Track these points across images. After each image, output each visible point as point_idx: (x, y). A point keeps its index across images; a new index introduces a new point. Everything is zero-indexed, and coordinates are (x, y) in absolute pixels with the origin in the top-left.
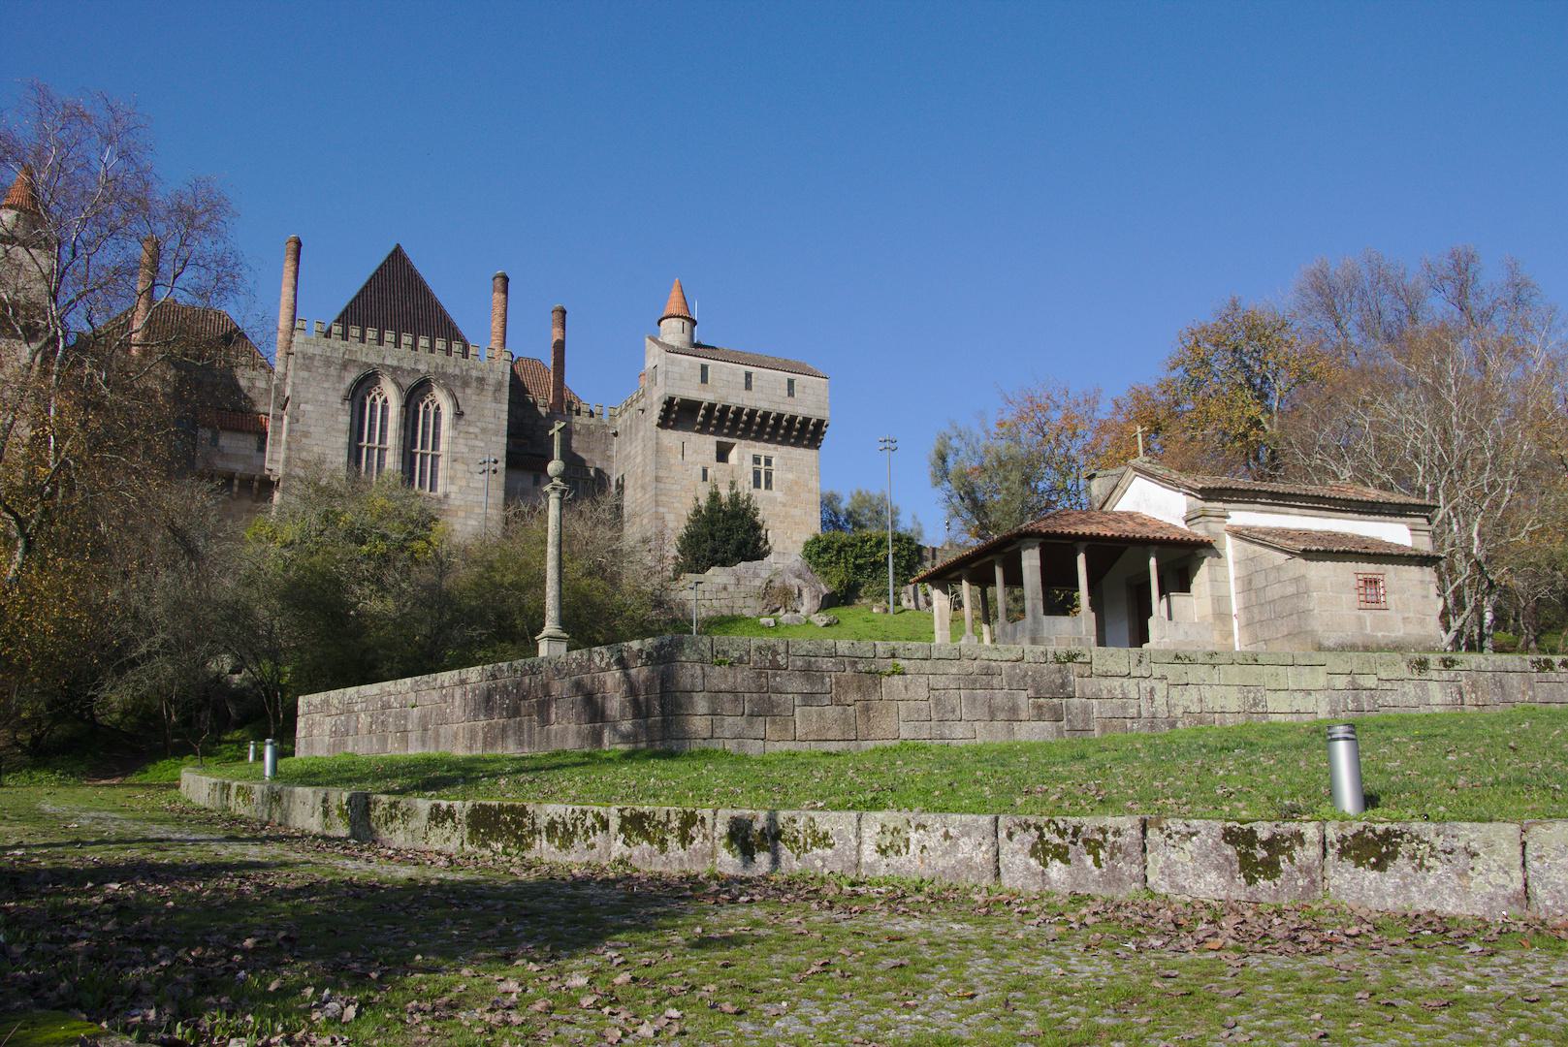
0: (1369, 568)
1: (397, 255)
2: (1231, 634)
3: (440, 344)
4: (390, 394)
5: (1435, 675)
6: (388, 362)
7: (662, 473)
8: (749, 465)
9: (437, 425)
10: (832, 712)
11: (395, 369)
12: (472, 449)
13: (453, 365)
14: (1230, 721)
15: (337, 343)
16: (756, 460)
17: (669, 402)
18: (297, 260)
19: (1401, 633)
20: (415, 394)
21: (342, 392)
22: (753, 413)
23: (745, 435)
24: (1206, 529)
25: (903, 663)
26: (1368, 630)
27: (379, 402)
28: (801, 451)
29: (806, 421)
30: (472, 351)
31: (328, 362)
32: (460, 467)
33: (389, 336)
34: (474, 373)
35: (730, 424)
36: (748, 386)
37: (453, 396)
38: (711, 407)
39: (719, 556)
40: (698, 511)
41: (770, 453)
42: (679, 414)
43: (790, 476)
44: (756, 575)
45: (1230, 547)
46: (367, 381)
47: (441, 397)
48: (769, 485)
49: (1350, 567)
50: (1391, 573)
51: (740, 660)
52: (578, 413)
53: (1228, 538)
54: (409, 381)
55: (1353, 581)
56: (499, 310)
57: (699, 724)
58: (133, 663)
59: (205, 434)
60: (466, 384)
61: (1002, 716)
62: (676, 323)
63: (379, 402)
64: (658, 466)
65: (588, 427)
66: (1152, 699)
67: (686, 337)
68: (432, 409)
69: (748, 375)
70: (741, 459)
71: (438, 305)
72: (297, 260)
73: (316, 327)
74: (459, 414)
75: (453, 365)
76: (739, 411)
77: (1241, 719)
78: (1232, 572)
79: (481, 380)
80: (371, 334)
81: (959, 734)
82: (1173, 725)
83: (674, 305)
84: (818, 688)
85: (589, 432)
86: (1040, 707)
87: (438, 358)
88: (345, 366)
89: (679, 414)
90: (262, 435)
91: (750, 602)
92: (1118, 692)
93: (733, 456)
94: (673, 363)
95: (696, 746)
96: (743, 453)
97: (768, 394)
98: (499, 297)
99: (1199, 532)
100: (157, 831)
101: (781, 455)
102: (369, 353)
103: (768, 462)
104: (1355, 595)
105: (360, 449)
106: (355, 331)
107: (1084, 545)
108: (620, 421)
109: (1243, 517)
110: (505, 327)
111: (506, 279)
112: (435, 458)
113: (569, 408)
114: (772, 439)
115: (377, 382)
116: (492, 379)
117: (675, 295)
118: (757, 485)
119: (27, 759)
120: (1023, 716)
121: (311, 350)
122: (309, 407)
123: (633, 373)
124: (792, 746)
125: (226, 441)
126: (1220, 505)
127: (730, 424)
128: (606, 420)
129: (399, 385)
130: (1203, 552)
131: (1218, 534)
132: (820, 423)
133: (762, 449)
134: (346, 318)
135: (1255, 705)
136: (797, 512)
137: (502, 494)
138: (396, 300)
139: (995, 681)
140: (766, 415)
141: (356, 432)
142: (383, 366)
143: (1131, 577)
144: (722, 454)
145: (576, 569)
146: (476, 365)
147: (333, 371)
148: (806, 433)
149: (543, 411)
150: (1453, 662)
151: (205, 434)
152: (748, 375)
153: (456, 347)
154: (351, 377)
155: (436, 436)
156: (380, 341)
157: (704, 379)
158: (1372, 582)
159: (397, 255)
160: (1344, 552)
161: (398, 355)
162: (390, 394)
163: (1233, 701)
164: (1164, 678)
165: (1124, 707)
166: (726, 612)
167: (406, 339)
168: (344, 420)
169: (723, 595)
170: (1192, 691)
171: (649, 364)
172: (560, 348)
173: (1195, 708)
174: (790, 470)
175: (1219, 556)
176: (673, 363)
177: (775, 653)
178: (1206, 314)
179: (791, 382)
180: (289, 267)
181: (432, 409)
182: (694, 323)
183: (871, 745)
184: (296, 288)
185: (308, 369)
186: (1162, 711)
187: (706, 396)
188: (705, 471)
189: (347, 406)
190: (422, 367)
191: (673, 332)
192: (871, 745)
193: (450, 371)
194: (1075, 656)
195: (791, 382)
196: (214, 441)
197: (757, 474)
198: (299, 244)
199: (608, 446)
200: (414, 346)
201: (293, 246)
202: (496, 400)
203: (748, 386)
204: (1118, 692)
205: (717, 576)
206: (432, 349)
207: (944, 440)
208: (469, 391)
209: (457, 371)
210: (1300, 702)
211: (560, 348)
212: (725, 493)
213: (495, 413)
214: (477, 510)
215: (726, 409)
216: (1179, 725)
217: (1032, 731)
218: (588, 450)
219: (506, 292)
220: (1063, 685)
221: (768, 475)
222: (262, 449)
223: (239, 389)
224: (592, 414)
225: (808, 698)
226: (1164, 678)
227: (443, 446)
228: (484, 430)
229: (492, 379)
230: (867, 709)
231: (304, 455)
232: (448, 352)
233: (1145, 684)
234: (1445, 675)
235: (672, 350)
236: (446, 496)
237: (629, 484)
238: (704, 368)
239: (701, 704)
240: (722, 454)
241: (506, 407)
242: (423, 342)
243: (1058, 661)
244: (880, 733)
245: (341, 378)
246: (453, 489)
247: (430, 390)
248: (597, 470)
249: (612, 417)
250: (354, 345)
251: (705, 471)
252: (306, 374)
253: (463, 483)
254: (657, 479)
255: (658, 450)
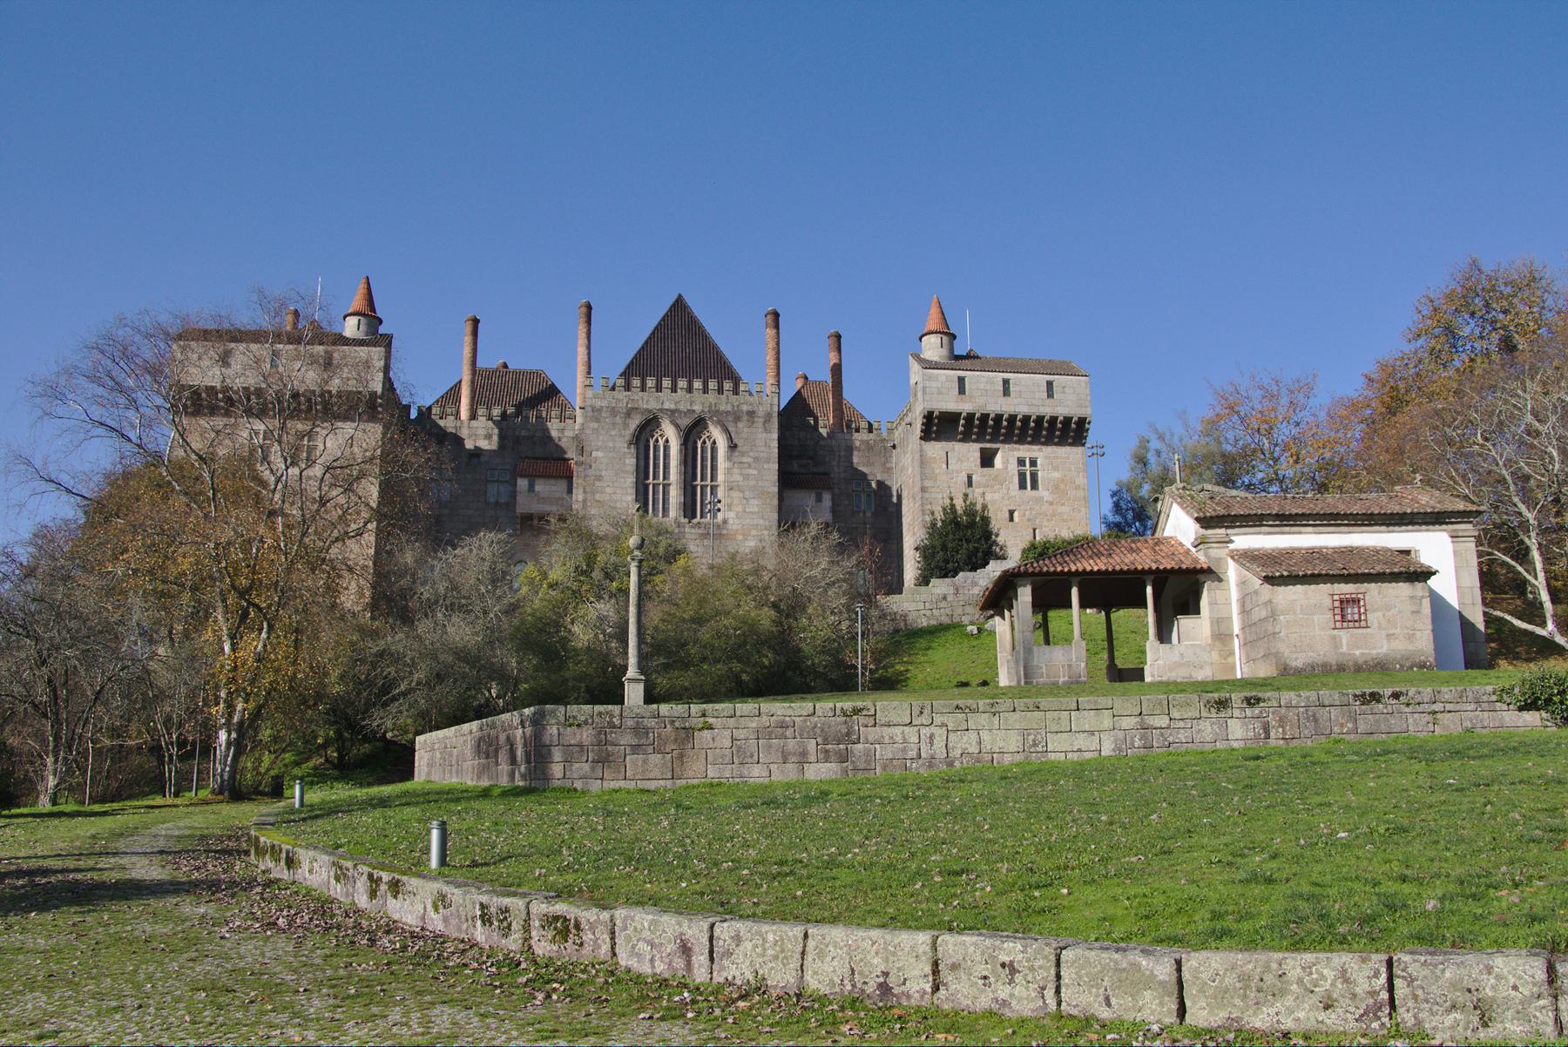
0: (1347, 589)
1: (679, 307)
2: (1232, 653)
3: (712, 384)
4: (670, 434)
5: (1237, 713)
6: (666, 406)
7: (927, 483)
8: (1013, 468)
9: (714, 458)
10: (655, 758)
11: (673, 412)
12: (746, 477)
13: (725, 403)
14: (1007, 759)
15: (621, 395)
16: (1021, 462)
17: (929, 417)
18: (589, 322)
19: (1384, 650)
20: (692, 432)
21: (628, 438)
22: (1012, 418)
23: (1008, 439)
24: (1206, 555)
25: (711, 720)
26: (1344, 649)
27: (661, 443)
28: (1067, 449)
29: (1067, 420)
30: (742, 388)
31: (613, 412)
32: (735, 494)
33: (666, 383)
34: (745, 408)
35: (990, 431)
36: (1006, 392)
37: (726, 430)
38: (970, 417)
39: (950, 566)
40: (933, 525)
41: (1034, 455)
42: (939, 426)
43: (1056, 475)
44: (975, 584)
45: (1232, 571)
46: (649, 425)
47: (716, 433)
48: (1035, 486)
49: (1325, 588)
50: (1373, 593)
51: (586, 722)
52: (857, 430)
53: (1231, 565)
54: (685, 422)
55: (1328, 602)
56: (771, 344)
57: (557, 770)
58: (394, 699)
59: (522, 483)
60: (737, 419)
61: (794, 759)
62: (933, 340)
63: (661, 443)
64: (923, 477)
65: (867, 442)
66: (932, 744)
67: (945, 352)
68: (709, 444)
69: (1006, 382)
70: (1006, 463)
71: (715, 347)
72: (589, 322)
73: (603, 382)
74: (733, 447)
75: (725, 403)
76: (999, 418)
77: (1019, 758)
78: (1234, 595)
79: (751, 414)
80: (651, 382)
81: (756, 774)
82: (951, 764)
83: (933, 322)
84: (643, 741)
85: (869, 447)
86: (827, 751)
87: (712, 397)
88: (629, 414)
89: (939, 426)
90: (568, 477)
91: (969, 609)
92: (899, 739)
93: (998, 460)
94: (930, 378)
95: (556, 783)
96: (1007, 457)
97: (1028, 397)
98: (771, 332)
99: (1202, 559)
100: (71, 864)
101: (1051, 459)
102: (649, 401)
103: (1033, 463)
104: (1329, 615)
105: (646, 487)
106: (636, 382)
107: (1075, 580)
108: (896, 434)
109: (1246, 540)
110: (778, 359)
111: (776, 315)
112: (714, 489)
113: (849, 427)
114: (1035, 441)
115: (659, 425)
116: (761, 411)
117: (934, 311)
118: (1022, 486)
119: (336, 772)
120: (812, 758)
121: (598, 403)
122: (600, 454)
123: (900, 388)
124: (622, 784)
125: (541, 486)
126: (1223, 531)
127: (990, 431)
128: (885, 435)
129: (677, 426)
130: (1201, 577)
131: (1219, 560)
132: (1082, 422)
133: (1026, 451)
134: (627, 374)
135: (1035, 745)
136: (1065, 509)
137: (776, 516)
138: (679, 347)
139: (789, 733)
140: (1026, 419)
141: (642, 472)
142: (661, 410)
143: (1180, 591)
144: (987, 460)
145: (655, 614)
146: (744, 403)
147: (618, 419)
148: (1070, 431)
149: (824, 432)
150: (1258, 700)
151: (522, 483)
152: (1006, 382)
153: (727, 385)
154: (635, 422)
155: (714, 468)
156: (659, 388)
157: (962, 390)
158: (1344, 602)
159: (679, 307)
160: (1313, 575)
161: (676, 399)
162: (670, 434)
163: (1012, 742)
164: (944, 725)
165: (904, 750)
166: (945, 620)
167: (682, 383)
168: (631, 462)
169: (943, 604)
170: (973, 736)
171: (912, 382)
172: (837, 370)
173: (974, 749)
174: (1056, 469)
175: (1220, 580)
176: (930, 378)
177: (612, 716)
178: (1440, 280)
179: (1050, 384)
180: (582, 328)
181: (709, 444)
182: (953, 337)
183: (684, 782)
184: (589, 347)
185: (598, 421)
186: (941, 753)
187: (965, 407)
188: (970, 478)
189: (633, 450)
190: (697, 408)
191: (932, 348)
192: (684, 782)
193: (722, 408)
194: (860, 710)
195: (1050, 384)
196: (531, 488)
197: (1022, 476)
198: (589, 307)
199: (887, 459)
200: (690, 390)
201: (584, 310)
202: (766, 430)
203: (1006, 392)
204: (899, 739)
205: (939, 586)
206: (705, 390)
207: (1144, 442)
208: (740, 425)
209: (729, 408)
210: (1081, 742)
211: (837, 370)
212: (959, 504)
213: (766, 442)
214: (754, 532)
215: (985, 417)
216: (957, 764)
217: (820, 772)
218: (869, 464)
219: (777, 327)
220: (848, 734)
221: (1034, 476)
222: (570, 491)
223: (550, 438)
224: (870, 429)
225: (636, 749)
226: (944, 725)
227: (721, 477)
228: (756, 459)
229: (761, 411)
230: (681, 756)
231: (598, 497)
232: (720, 390)
233: (925, 731)
234: (1249, 712)
235: (929, 365)
236: (725, 522)
237: (905, 494)
238: (961, 380)
239: (557, 755)
240: (987, 460)
241: (775, 436)
242: (697, 384)
243: (845, 715)
244: (691, 774)
245: (626, 425)
246: (731, 515)
247: (706, 427)
248: (880, 483)
249: (891, 430)
250: (636, 394)
251: (970, 478)
252: (596, 425)
253: (740, 509)
254: (923, 490)
255: (923, 462)
